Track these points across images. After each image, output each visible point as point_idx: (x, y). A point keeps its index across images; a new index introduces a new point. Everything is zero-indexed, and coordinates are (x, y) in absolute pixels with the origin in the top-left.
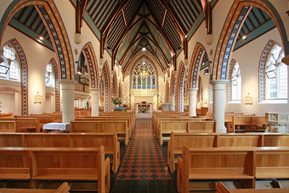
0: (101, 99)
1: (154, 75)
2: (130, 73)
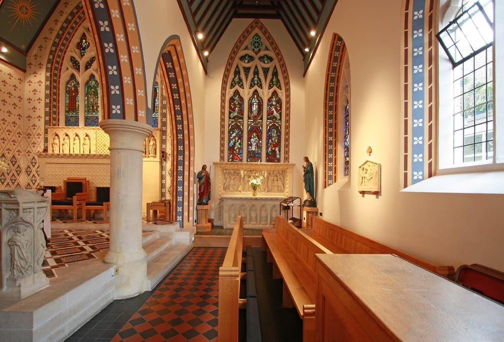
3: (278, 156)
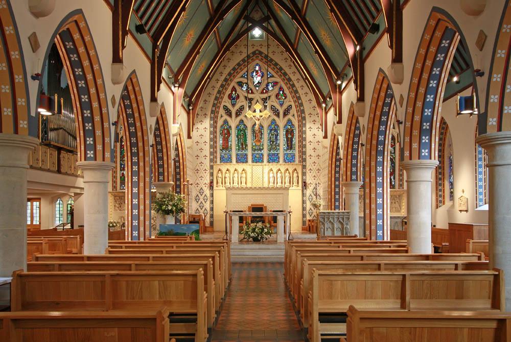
0: (115, 196)
1: (289, 116)
2: (212, 112)
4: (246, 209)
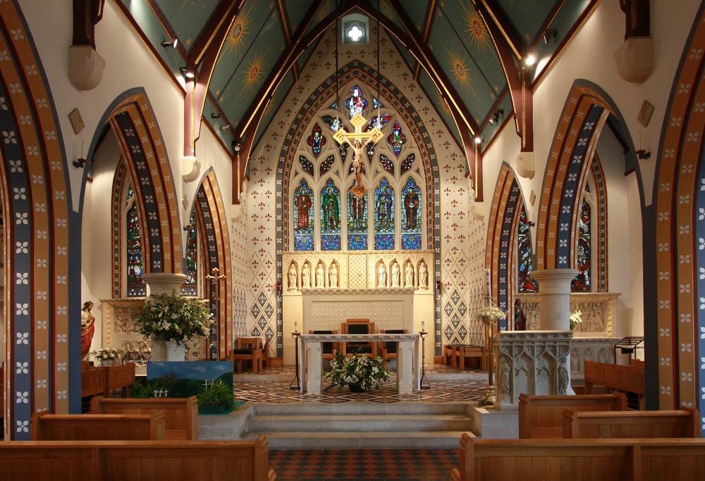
0: (116, 308)
1: (412, 173)
2: (280, 165)
3: (588, 283)
4: (338, 327)
